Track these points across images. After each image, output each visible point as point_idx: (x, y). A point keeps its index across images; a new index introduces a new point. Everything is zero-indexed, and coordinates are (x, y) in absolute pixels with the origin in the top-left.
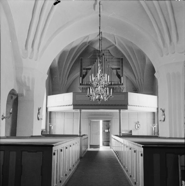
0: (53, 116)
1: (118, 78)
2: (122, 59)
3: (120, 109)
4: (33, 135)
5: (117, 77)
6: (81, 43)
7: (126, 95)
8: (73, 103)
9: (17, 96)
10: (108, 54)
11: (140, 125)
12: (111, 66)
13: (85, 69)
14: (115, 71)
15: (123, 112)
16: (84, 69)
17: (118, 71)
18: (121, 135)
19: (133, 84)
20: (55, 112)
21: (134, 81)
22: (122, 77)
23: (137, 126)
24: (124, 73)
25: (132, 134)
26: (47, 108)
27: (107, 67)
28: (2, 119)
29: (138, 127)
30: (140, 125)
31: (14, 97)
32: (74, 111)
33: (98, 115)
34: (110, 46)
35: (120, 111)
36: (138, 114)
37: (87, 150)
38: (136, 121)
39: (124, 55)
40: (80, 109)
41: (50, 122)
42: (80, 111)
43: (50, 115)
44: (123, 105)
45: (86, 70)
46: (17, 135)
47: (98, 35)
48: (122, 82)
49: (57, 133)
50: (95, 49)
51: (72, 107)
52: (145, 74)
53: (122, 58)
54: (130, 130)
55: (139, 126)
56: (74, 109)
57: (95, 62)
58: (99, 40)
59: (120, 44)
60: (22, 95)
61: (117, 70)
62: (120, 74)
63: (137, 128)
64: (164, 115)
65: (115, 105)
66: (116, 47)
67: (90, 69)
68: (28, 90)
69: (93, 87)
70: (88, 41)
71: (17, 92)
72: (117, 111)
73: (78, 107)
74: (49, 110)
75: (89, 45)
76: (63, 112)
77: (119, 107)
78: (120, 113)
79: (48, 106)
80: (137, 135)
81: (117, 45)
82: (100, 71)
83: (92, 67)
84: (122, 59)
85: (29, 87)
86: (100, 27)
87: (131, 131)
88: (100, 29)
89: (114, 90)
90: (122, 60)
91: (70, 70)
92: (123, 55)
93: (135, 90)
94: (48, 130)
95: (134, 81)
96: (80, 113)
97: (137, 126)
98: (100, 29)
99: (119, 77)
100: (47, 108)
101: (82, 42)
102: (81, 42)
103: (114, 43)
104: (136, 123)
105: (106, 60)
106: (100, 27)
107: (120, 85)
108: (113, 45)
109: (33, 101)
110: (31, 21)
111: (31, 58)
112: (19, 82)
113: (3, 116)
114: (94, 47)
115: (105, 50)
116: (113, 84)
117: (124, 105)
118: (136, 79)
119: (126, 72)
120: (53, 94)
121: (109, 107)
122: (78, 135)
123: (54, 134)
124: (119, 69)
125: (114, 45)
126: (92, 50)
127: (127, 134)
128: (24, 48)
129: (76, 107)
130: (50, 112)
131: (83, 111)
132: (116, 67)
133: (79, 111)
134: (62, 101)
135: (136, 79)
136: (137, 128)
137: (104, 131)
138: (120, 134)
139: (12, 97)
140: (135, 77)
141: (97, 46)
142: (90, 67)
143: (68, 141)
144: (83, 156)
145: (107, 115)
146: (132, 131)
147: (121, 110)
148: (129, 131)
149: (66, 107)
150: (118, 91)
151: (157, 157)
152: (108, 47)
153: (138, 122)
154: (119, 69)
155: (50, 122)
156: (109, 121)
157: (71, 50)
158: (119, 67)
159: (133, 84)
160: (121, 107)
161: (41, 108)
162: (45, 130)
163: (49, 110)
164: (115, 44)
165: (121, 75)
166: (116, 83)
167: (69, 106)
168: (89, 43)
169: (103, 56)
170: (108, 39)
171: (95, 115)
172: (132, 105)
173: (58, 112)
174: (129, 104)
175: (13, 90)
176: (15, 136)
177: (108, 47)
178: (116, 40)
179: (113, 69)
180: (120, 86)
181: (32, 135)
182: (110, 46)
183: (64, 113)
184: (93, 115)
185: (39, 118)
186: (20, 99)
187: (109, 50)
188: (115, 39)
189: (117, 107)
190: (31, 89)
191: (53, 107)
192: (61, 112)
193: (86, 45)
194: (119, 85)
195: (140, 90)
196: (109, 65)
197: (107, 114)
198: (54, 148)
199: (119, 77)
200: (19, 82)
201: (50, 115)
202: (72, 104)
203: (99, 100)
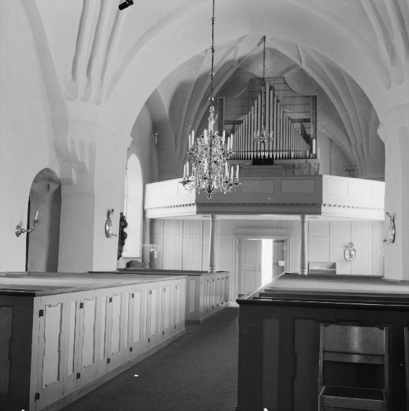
0: (158, 228)
1: (305, 143)
2: (315, 98)
3: (303, 214)
4: (94, 271)
5: (302, 141)
6: (222, 64)
7: (317, 180)
8: (196, 200)
9: (59, 184)
10: (282, 87)
11: (354, 250)
12: (289, 115)
13: (228, 124)
14: (298, 126)
15: (311, 220)
16: (227, 123)
17: (306, 125)
18: (306, 273)
19: (344, 155)
20: (163, 221)
21: (348, 148)
22: (314, 140)
23: (347, 253)
24: (318, 128)
25: (335, 272)
26: (144, 212)
27: (280, 116)
28: (18, 234)
29: (351, 256)
30: (354, 250)
31: (53, 187)
32: (200, 217)
33: (262, 227)
34: (288, 69)
35: (303, 218)
36: (352, 225)
37: (224, 303)
38: (347, 241)
39: (320, 87)
40: (213, 213)
41: (152, 242)
42: (213, 218)
43: (151, 227)
44: (312, 205)
45: (232, 126)
46: (61, 269)
47: (259, 44)
48: (314, 152)
49: (168, 266)
50: (254, 75)
51: (194, 208)
52: (349, 134)
53: (316, 96)
54: (331, 261)
55: (352, 252)
56: (198, 213)
57: (253, 107)
58: (211, 50)
59: (311, 63)
60: (70, 182)
61: (304, 124)
62: (311, 132)
63: (347, 257)
64: (394, 228)
65: (291, 205)
66: (302, 70)
67: (242, 122)
68: (82, 170)
69: (195, 161)
70: (237, 58)
71: (58, 173)
72: (297, 218)
73: (208, 209)
74: (150, 215)
75: (239, 69)
76: (179, 220)
77: (213, 209)
78: (303, 222)
79: (146, 207)
80: (349, 273)
81: (304, 66)
82: (212, 123)
83: (245, 118)
84: (315, 98)
85: (83, 164)
86: (213, 21)
87: (334, 266)
88: (213, 24)
89: (296, 170)
90: (314, 100)
91: (198, 122)
92: (320, 89)
93: (349, 171)
94: (148, 260)
95: (348, 148)
96: (213, 221)
97: (347, 253)
98: (213, 24)
99: (308, 139)
100: (144, 212)
101: (224, 62)
102: (221, 61)
103: (298, 62)
104: (347, 247)
105: (278, 101)
106: (213, 21)
107: (309, 158)
108: (296, 66)
109: (92, 195)
110: (81, 19)
111: (84, 100)
112: (61, 153)
113: (18, 227)
114: (251, 71)
115: (275, 78)
116: (292, 156)
117: (313, 205)
118: (350, 144)
119: (324, 126)
120: (160, 180)
121: (285, 209)
122: (207, 272)
123: (161, 269)
124: (307, 121)
125: (298, 66)
126: (249, 78)
127: (324, 271)
128: (71, 77)
129: (204, 209)
130: (152, 221)
131: (219, 217)
132: (302, 116)
133: (209, 217)
134: (172, 197)
135: (350, 144)
136: (347, 257)
137: (278, 264)
138: (303, 272)
139: (49, 186)
140: (349, 141)
141: (258, 70)
142: (240, 119)
143: (137, 281)
144: (201, 319)
145: (277, 227)
146: (337, 265)
147: (307, 216)
148: (329, 265)
149: (182, 208)
150: (306, 171)
151: (271, 327)
152: (284, 72)
153: (352, 244)
154: (307, 121)
155: (152, 242)
156: (283, 241)
157: (198, 79)
158: (308, 118)
159: (344, 155)
160: (217, 209)
161: (113, 210)
162: (140, 261)
163: (150, 215)
164: (299, 64)
165: (311, 137)
166: (301, 154)
167: (189, 208)
168: (241, 63)
169: (271, 92)
170: (283, 52)
171: (251, 227)
172: (347, 204)
173: (168, 220)
174: (324, 202)
175: (47, 170)
176: (56, 271)
177: (284, 72)
178: (301, 53)
179: (293, 121)
180: (309, 161)
181: (90, 270)
182: (288, 69)
183: (181, 222)
184: (246, 227)
185: (110, 232)
186: (64, 190)
187: (284, 78)
188: (298, 52)
189: (298, 209)
190: (88, 169)
191: (187, 205)
192: (177, 220)
193: (232, 67)
194: (306, 158)
195: (360, 170)
196: (284, 112)
197: (279, 226)
198: (36, 299)
199: (308, 139)
200: (61, 153)
201: (151, 227)
202: (194, 202)
203: (210, 191)
